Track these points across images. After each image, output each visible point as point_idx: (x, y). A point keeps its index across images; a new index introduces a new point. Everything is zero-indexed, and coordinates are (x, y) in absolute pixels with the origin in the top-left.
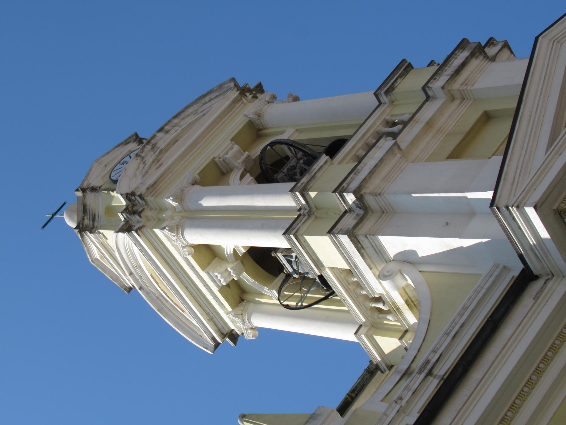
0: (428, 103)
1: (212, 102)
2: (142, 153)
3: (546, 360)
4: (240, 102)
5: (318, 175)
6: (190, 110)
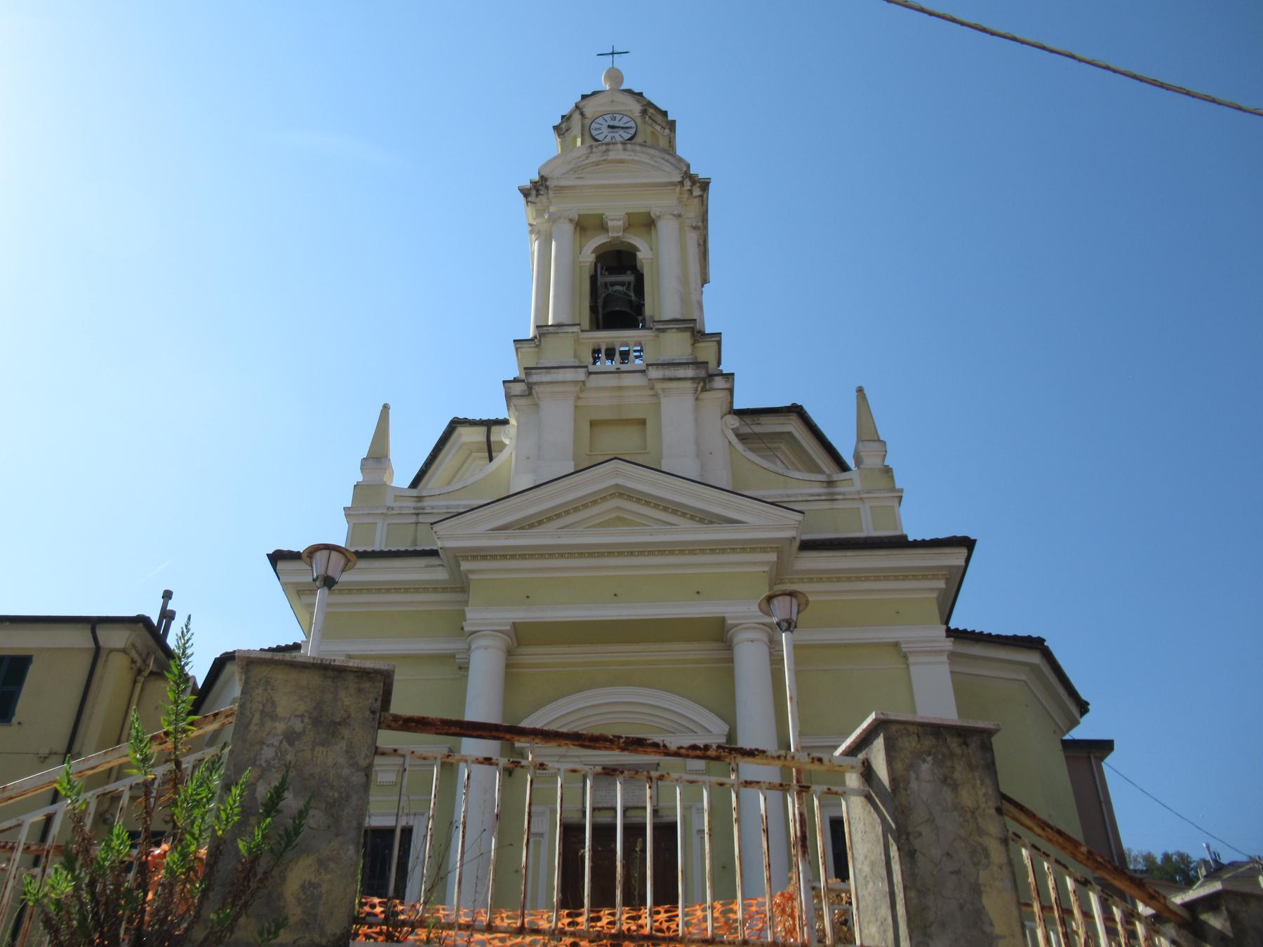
0: (640, 374)
2: (596, 147)
3: (674, 512)
4: (674, 188)
5: (560, 335)
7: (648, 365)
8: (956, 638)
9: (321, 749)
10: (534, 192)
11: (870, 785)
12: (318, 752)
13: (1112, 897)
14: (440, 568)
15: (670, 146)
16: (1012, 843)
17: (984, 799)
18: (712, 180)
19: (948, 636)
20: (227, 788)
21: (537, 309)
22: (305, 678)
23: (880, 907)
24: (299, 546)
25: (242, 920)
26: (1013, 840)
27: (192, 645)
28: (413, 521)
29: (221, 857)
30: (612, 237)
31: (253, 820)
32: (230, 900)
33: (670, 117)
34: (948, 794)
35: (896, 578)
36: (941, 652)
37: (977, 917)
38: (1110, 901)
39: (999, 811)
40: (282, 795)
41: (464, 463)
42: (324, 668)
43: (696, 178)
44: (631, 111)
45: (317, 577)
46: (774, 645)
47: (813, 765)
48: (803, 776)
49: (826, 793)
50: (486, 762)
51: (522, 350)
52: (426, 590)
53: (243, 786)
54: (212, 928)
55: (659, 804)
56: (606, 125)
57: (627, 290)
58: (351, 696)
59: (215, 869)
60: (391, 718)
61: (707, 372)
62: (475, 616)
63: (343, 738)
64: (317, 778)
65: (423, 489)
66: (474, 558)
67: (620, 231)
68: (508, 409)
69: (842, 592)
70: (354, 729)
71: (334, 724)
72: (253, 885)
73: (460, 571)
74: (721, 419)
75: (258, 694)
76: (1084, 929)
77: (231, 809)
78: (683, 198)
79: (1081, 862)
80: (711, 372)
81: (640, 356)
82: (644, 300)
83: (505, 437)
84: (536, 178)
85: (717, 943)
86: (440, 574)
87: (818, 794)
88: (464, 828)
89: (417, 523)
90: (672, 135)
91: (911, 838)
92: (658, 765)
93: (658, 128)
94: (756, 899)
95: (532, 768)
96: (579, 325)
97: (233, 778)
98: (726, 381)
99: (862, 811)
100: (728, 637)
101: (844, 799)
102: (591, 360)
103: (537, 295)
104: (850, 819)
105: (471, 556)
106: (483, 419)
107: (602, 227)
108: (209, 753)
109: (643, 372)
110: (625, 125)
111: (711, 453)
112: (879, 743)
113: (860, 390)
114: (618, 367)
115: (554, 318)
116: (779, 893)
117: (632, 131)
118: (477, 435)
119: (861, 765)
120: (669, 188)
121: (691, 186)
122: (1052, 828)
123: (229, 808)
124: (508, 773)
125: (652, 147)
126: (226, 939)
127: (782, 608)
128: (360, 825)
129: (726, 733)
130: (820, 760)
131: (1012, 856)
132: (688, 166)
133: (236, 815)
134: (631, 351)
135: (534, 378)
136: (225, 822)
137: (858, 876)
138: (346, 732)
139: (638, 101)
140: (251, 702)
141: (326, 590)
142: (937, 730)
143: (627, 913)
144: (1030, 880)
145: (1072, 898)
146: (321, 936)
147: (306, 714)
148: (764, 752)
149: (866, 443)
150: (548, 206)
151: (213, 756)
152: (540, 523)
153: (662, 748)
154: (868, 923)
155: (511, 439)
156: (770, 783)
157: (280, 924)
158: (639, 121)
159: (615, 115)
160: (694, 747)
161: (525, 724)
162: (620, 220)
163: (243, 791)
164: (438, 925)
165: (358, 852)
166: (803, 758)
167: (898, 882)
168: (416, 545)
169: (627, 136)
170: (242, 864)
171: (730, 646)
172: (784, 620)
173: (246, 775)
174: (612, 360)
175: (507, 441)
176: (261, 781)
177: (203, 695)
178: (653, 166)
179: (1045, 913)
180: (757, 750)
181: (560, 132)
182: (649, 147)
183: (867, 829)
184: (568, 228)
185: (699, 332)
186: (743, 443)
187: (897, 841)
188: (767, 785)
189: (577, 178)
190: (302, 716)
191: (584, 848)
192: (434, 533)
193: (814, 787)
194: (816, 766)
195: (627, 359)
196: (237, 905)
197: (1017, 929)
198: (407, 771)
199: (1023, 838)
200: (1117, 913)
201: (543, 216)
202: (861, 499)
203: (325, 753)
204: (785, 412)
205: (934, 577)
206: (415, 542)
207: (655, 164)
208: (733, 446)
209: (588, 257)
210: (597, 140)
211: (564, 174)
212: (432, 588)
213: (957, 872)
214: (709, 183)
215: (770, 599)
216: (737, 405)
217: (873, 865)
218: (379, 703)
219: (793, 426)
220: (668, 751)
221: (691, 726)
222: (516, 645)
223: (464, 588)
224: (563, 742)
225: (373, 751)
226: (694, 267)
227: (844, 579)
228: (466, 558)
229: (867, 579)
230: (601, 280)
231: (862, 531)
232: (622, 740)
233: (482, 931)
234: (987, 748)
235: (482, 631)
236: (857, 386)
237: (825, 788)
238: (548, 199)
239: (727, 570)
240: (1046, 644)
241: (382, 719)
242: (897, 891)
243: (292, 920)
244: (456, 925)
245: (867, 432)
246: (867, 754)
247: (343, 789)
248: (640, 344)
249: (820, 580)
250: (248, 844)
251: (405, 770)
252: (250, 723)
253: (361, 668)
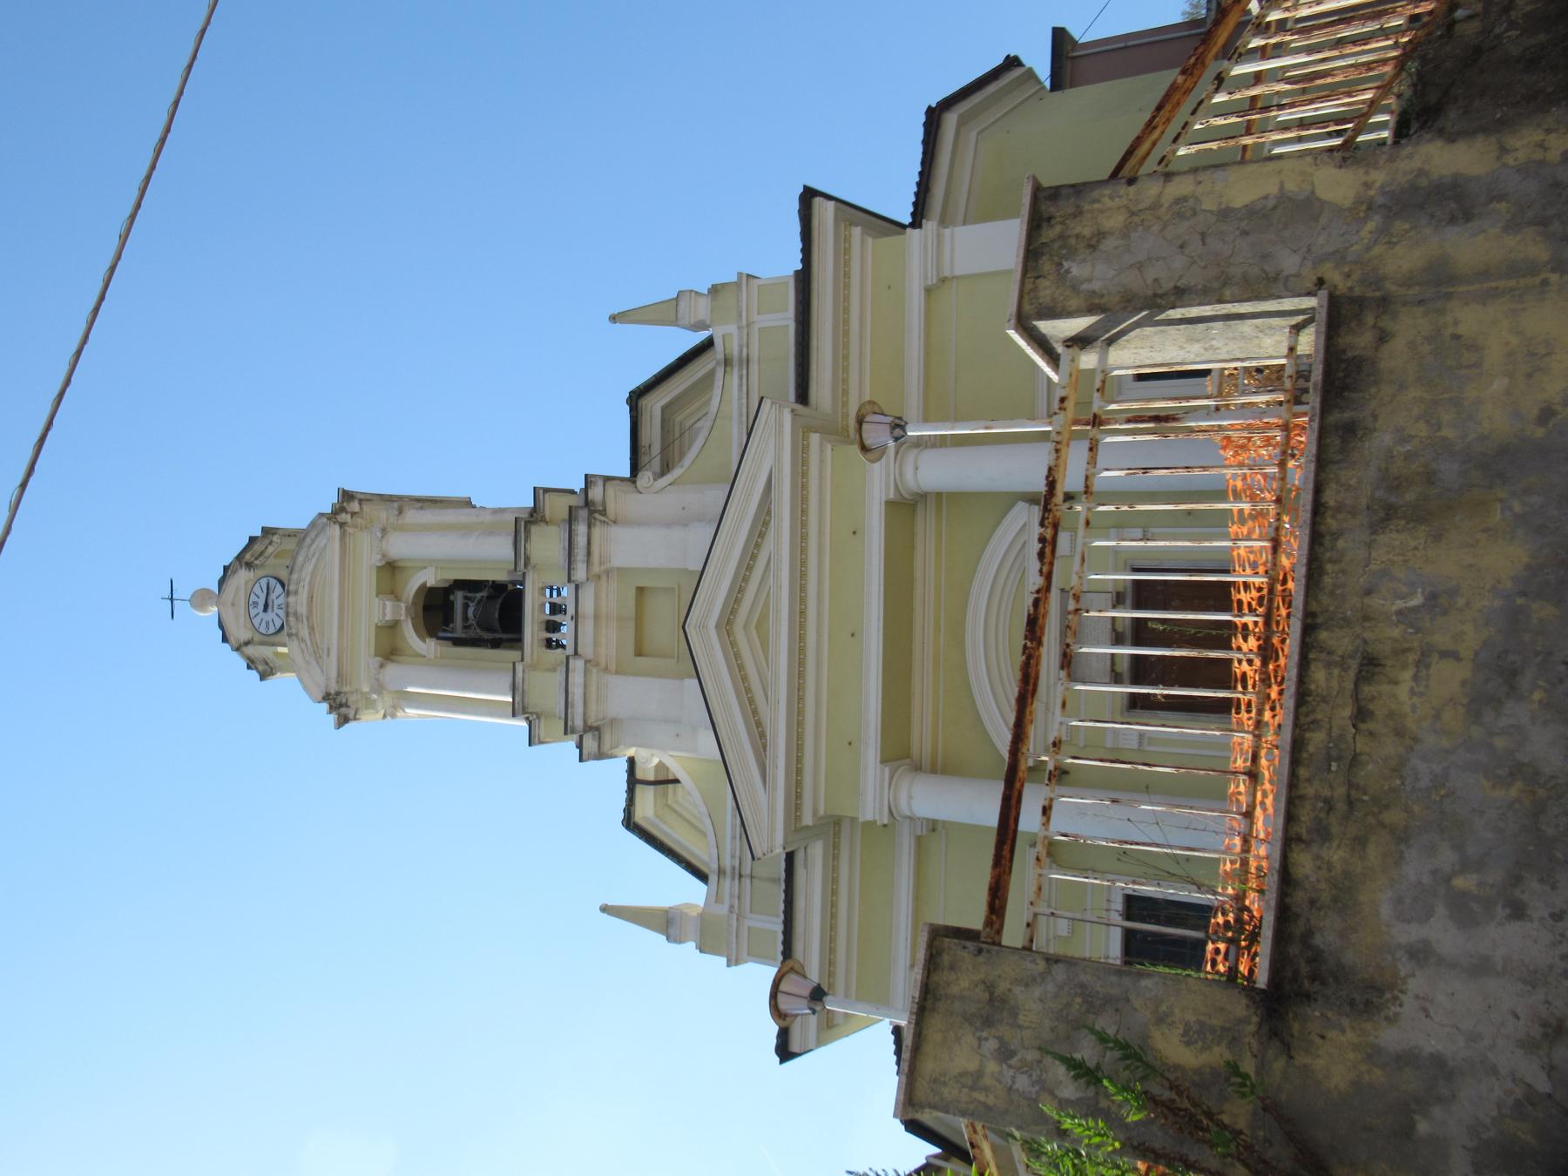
0: (580, 591)
1: (316, 542)
2: (291, 628)
3: (754, 557)
4: (348, 535)
5: (526, 687)
7: (569, 580)
8: (922, 217)
9: (1021, 1017)
10: (343, 710)
11: (1096, 339)
12: (1025, 1021)
13: (1237, 48)
14: (809, 851)
15: (295, 536)
16: (1170, 168)
17: (1117, 200)
18: (341, 486)
19: (920, 226)
20: (1063, 1134)
21: (491, 715)
22: (934, 1035)
23: (1242, 333)
24: (774, 1029)
25: (1226, 1119)
26: (1167, 166)
27: (884, 1170)
28: (748, 881)
29: (1147, 1144)
30: (406, 616)
31: (1104, 1103)
32: (1201, 1134)
33: (258, 533)
34: (1109, 244)
35: (847, 286)
36: (939, 237)
37: (1257, 216)
38: (1242, 50)
39: (1131, 181)
40: (1078, 1062)
41: (680, 815)
42: (927, 1001)
43: (337, 507)
44: (246, 583)
45: (810, 1009)
46: (920, 443)
47: (1068, 410)
48: (1081, 417)
49: (1103, 394)
50: (1048, 812)
51: (542, 736)
52: (835, 869)
53: (1063, 1114)
54: (1232, 1157)
55: (1110, 590)
56: (262, 615)
57: (473, 601)
58: (958, 979)
59: (1161, 1152)
60: (988, 930)
61: (581, 507)
62: (870, 809)
63: (1010, 990)
64: (1056, 1024)
65: (710, 867)
66: (798, 808)
67: (400, 606)
68: (615, 757)
69: (861, 337)
70: (1000, 976)
71: (991, 1000)
72: (1186, 1104)
73: (814, 826)
74: (641, 493)
75: (950, 1093)
76: (1274, 84)
77: (1089, 1129)
78: (361, 524)
79: (1196, 83)
80: (581, 502)
81: (558, 589)
82: (488, 581)
83: (649, 761)
84: (325, 706)
85: (1278, 535)
86: (817, 850)
87: (1103, 403)
88: (1126, 843)
89: (752, 877)
90: (281, 532)
91: (1160, 292)
92: (1062, 590)
93: (271, 549)
94: (1228, 480)
95: (1058, 757)
96: (514, 664)
97: (1051, 1127)
99: (1126, 350)
100: (910, 498)
101: (1112, 372)
102: (560, 650)
103: (476, 714)
104: (1136, 364)
105: (796, 812)
106: (626, 788)
107: (393, 626)
108: (1019, 1155)
109: (577, 587)
110: (265, 591)
111: (683, 508)
112: (1045, 326)
113: (614, 319)
114: (570, 617)
115: (504, 694)
116: (1222, 452)
117: (273, 582)
118: (646, 797)
119: (1071, 350)
120: (347, 540)
121: (347, 513)
122: (1154, 117)
123: (1087, 1132)
124: (1064, 776)
125: (294, 559)
126: (1249, 1140)
127: (876, 434)
128: (1118, 972)
129: (1027, 505)
130: (1063, 400)
131: (1186, 169)
132: (321, 515)
133: (1097, 1124)
134: (551, 600)
135: (579, 723)
136: (1105, 1138)
137: (1203, 358)
138: (1002, 986)
139: (235, 573)
140: (959, 1102)
141: (827, 999)
142: (1032, 253)
143: (1239, 592)
144: (1215, 147)
145: (1237, 96)
146: (1250, 1023)
147: (978, 1034)
148: (1050, 469)
149: (680, 315)
150: (362, 693)
151: (1023, 1150)
152: (759, 724)
153: (1040, 595)
154: (1260, 347)
155: (652, 755)
156: (1088, 463)
157: (1234, 1068)
158: (260, 573)
159: (251, 602)
160: (1041, 555)
161: (1005, 751)
162: (384, 605)
163: (1068, 1115)
164: (1243, 878)
165: (1149, 975)
166: (1060, 418)
167: (1213, 310)
168: (779, 879)
169: (279, 589)
170: (1156, 1117)
171: (922, 496)
172: (892, 433)
173: (1049, 1109)
174: (561, 624)
175: (655, 761)
176: (1056, 1092)
177: (952, 1149)
178: (318, 559)
179: (1253, 131)
180: (1047, 477)
181: (268, 673)
182: (294, 563)
183: (1148, 345)
184: (392, 671)
185: (532, 515)
186: (673, 467)
187: (1163, 309)
188: (1090, 466)
189: (328, 655)
190: (980, 1039)
191: (1155, 695)
192: (765, 857)
193: (1095, 409)
194: (1070, 404)
195: (561, 606)
196: (1208, 1125)
197: (1271, 166)
198: (1055, 911)
199: (1165, 153)
200: (1256, 42)
201: (375, 700)
202: (748, 325)
203: (1027, 1013)
204: (637, 414)
205: (848, 239)
206: (776, 881)
207: (316, 556)
208: (675, 480)
209: (430, 647)
210: (282, 627)
211: (323, 672)
212: (833, 861)
213: (1203, 236)
214: (344, 491)
215: (864, 449)
216: (626, 472)
217: (1191, 340)
218: (969, 944)
219: (654, 404)
220: (1045, 588)
221: (1019, 546)
222: (908, 761)
223: (834, 823)
224: (1028, 717)
225: (1027, 953)
226: (449, 516)
227: (845, 352)
228: (798, 818)
229: (846, 322)
230: (459, 633)
231: (788, 326)
232: (1029, 644)
233: (1252, 824)
234: (1055, 193)
236: (610, 324)
237: (1096, 395)
238: (352, 692)
239: (828, 530)
240: (934, 105)
241: (989, 940)
242: (1224, 312)
243: (1228, 1056)
244: (1243, 855)
245: (665, 313)
246: (1057, 342)
247: (1072, 991)
248: (543, 589)
249: (845, 381)
250: (1134, 1109)
251: (1053, 914)
252: (985, 1105)
253: (924, 965)
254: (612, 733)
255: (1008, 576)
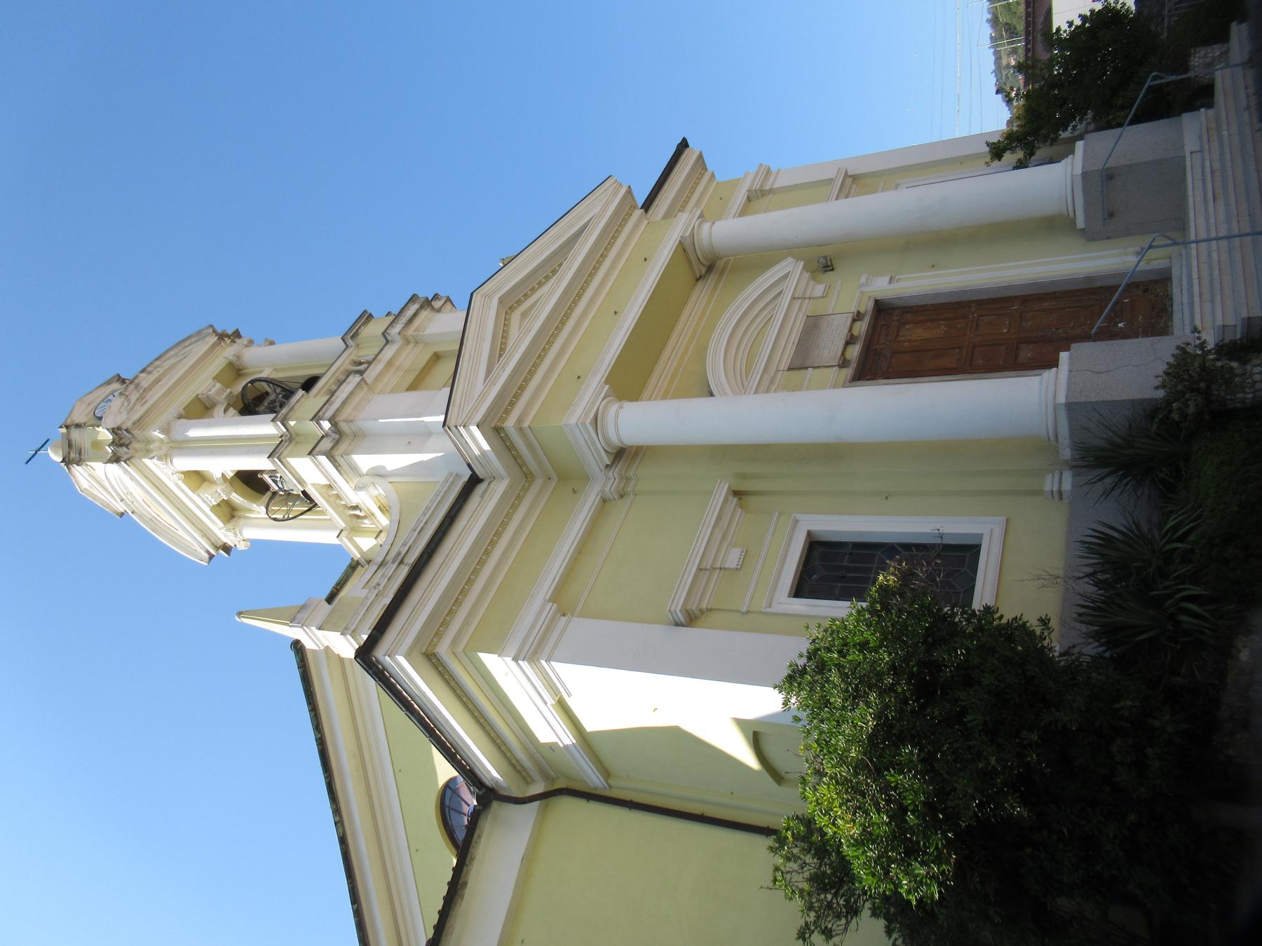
5: (297, 406)
6: (172, 353)
14: (492, 485)
30: (226, 398)
98: (439, 300)
189: (143, 405)
235: (599, 407)
254: (350, 445)
255: (761, 311)
